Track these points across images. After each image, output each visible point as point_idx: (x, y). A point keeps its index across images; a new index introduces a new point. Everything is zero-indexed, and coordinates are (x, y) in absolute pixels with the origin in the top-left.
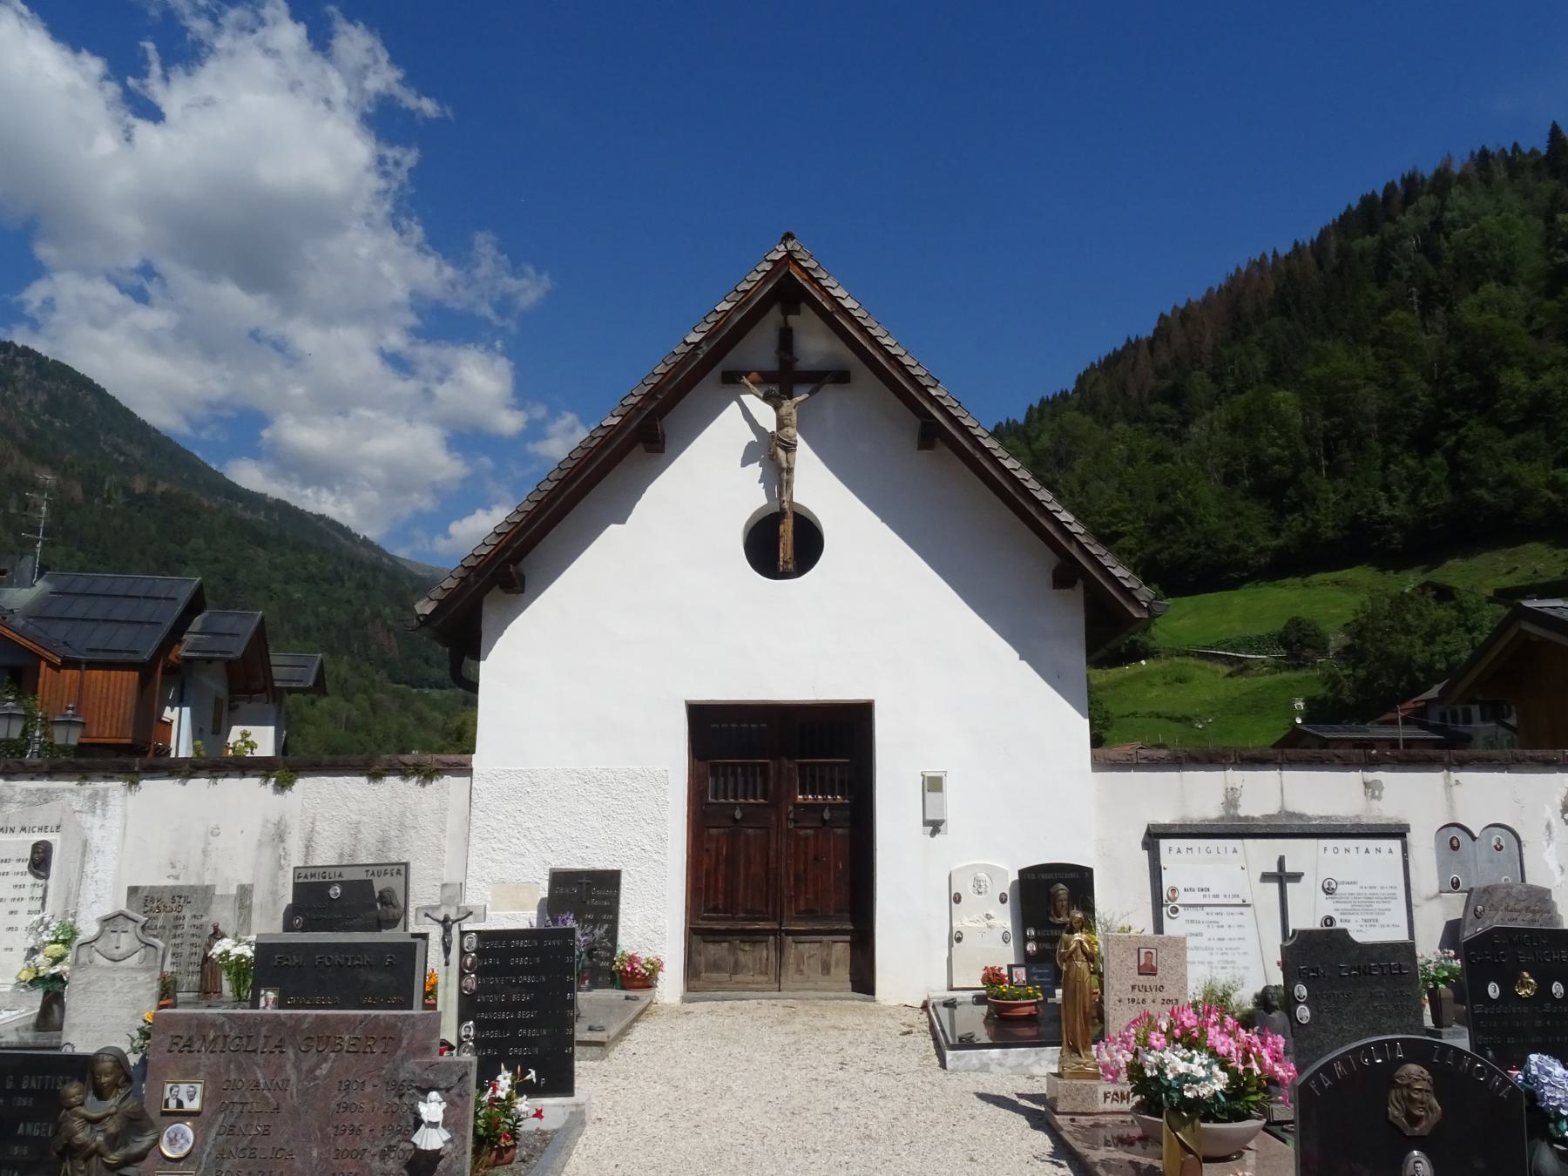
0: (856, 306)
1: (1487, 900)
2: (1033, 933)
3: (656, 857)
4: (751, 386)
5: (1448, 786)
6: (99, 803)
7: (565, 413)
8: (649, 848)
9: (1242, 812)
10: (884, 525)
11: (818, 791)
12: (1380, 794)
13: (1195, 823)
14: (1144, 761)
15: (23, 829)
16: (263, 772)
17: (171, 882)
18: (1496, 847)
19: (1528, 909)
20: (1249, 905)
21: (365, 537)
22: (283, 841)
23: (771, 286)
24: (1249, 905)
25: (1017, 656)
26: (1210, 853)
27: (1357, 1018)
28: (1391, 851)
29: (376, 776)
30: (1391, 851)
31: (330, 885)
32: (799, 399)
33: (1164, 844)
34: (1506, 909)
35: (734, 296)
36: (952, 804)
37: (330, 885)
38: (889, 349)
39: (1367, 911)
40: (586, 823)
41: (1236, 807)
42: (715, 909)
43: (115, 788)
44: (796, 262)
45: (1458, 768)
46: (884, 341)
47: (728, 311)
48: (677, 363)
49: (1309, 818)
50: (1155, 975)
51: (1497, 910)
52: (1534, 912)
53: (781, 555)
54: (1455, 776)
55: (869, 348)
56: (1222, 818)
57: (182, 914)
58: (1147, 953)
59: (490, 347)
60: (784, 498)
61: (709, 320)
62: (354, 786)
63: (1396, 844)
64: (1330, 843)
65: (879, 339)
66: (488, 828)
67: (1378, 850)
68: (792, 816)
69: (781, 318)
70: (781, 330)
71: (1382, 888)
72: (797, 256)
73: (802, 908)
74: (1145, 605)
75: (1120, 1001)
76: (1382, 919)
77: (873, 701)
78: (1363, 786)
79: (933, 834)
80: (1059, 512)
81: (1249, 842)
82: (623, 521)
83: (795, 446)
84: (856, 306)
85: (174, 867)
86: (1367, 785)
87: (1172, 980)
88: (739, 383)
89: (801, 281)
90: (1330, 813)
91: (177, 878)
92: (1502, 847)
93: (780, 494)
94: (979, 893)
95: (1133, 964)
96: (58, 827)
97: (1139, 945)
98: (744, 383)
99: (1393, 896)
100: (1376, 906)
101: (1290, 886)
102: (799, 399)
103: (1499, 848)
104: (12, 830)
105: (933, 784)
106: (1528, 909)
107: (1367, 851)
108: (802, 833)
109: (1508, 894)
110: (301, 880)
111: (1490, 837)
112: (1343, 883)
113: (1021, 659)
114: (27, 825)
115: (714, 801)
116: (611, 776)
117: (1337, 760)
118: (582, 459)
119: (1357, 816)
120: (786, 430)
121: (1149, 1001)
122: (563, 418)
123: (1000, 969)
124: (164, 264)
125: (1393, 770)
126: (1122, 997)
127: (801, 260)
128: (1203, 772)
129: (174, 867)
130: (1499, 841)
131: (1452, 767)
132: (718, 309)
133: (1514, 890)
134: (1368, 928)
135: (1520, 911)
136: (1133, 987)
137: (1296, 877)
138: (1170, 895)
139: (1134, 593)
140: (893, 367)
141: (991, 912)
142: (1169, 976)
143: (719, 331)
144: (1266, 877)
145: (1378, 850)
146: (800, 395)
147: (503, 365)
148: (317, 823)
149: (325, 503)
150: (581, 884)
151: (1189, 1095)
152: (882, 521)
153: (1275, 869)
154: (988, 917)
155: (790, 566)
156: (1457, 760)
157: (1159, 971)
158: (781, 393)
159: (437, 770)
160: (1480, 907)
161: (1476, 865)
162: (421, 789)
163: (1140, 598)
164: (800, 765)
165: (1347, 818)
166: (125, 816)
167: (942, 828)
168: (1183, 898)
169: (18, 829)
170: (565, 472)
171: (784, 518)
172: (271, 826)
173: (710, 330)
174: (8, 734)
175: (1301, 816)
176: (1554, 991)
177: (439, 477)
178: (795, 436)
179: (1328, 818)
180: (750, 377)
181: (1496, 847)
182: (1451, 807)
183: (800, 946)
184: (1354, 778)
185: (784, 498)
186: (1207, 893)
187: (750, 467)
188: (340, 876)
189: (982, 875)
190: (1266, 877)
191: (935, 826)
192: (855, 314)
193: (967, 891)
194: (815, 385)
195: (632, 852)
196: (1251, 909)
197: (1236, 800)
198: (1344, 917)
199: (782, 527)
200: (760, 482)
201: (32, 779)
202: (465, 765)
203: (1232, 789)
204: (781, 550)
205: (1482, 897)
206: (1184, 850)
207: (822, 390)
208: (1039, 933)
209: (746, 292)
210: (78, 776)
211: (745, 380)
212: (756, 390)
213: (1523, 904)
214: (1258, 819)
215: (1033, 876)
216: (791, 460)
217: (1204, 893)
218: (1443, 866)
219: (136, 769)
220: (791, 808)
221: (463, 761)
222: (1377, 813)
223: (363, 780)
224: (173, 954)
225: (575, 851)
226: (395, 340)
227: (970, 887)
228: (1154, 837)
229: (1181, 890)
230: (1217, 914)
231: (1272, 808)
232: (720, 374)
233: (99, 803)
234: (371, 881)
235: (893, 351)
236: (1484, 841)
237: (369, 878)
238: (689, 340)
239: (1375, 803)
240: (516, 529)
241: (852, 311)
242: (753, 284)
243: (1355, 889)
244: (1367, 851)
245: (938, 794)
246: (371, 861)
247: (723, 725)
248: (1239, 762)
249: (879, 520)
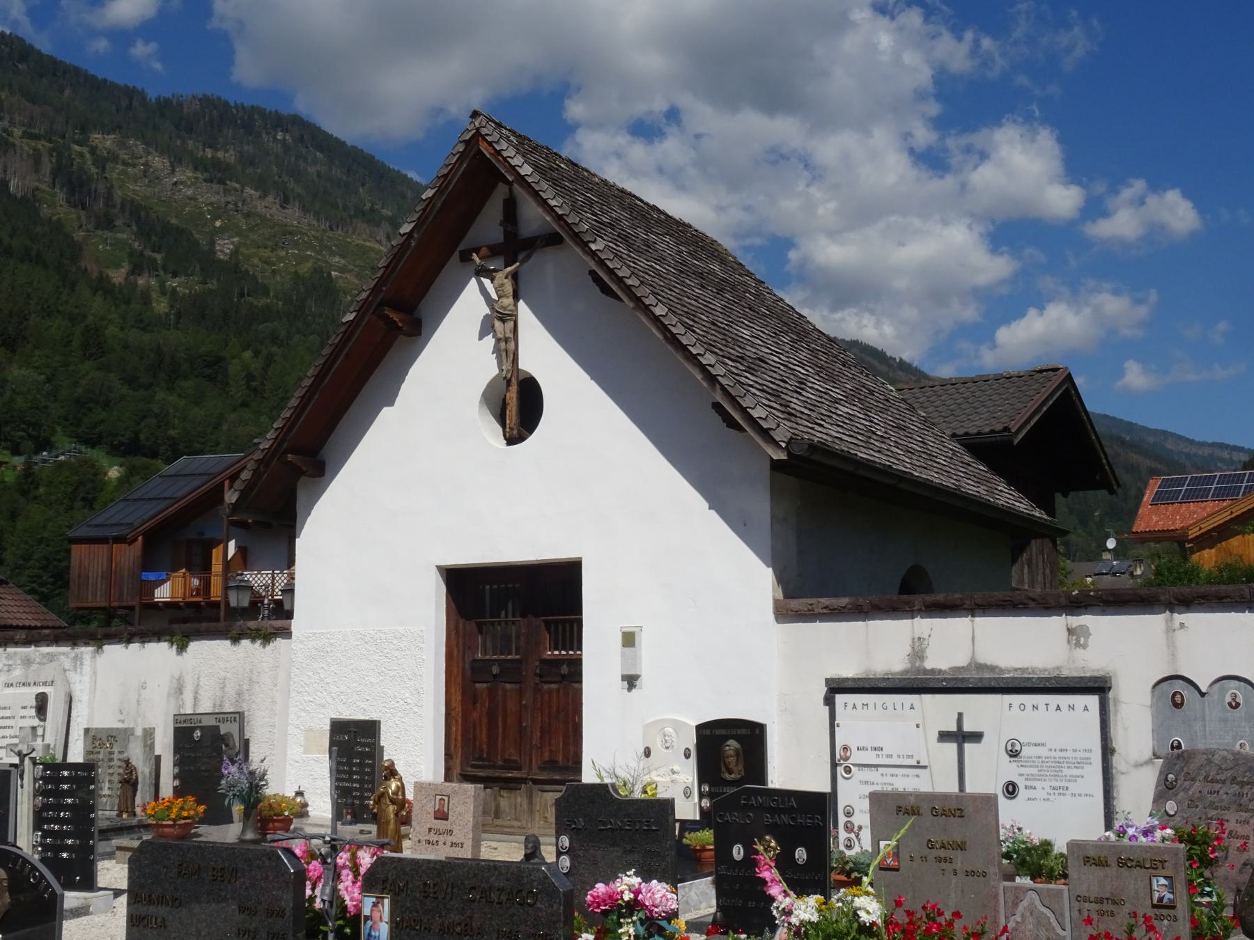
1: (1182, 769)
2: (707, 789)
3: (415, 709)
5: (1170, 631)
6: (79, 663)
7: (1132, 181)
8: (409, 701)
9: (929, 665)
10: (593, 382)
11: (568, 647)
12: (1086, 641)
13: (878, 676)
14: (825, 611)
15: (35, 684)
16: (168, 638)
17: (120, 725)
18: (1230, 704)
19: (1234, 779)
20: (925, 767)
21: (901, 359)
22: (181, 693)
24: (925, 767)
25: (707, 505)
26: (886, 709)
27: (611, 871)
28: (1086, 709)
29: (236, 640)
30: (1086, 709)
31: (194, 729)
33: (840, 699)
34: (1206, 778)
36: (648, 661)
37: (193, 729)
39: (1056, 777)
40: (366, 678)
41: (922, 658)
42: (481, 759)
43: (86, 651)
44: (483, 137)
45: (1183, 608)
46: (553, 203)
49: (1002, 671)
50: (447, 819)
51: (1193, 780)
52: (1242, 784)
54: (1178, 618)
56: (906, 672)
57: (113, 750)
58: (441, 799)
59: (1028, 119)
62: (221, 647)
63: (1093, 701)
64: (1016, 699)
66: (302, 683)
67: (1071, 707)
68: (538, 671)
71: (1075, 751)
72: (484, 131)
73: (547, 759)
74: (783, 445)
75: (419, 841)
76: (1074, 788)
77: (581, 558)
78: (1066, 633)
79: (630, 689)
80: (702, 355)
81: (927, 698)
82: (391, 403)
85: (121, 714)
86: (1070, 631)
87: (460, 825)
90: (1026, 665)
91: (123, 722)
92: (1238, 705)
94: (667, 748)
95: (432, 811)
96: (52, 682)
97: (436, 792)
99: (1087, 761)
100: (1066, 772)
101: (968, 747)
103: (1235, 706)
104: (29, 685)
105: (629, 639)
106: (1234, 779)
107: (1058, 708)
108: (546, 687)
109: (1209, 761)
110: (178, 725)
111: (1223, 692)
112: (1029, 744)
113: (710, 508)
114: (37, 680)
115: (483, 658)
116: (383, 636)
117: (1032, 604)
118: (331, 354)
119: (1058, 668)
121: (441, 843)
122: (1130, 186)
124: (685, 100)
125: (1103, 613)
126: (421, 838)
127: (487, 135)
128: (889, 621)
129: (121, 714)
130: (1234, 696)
131: (1177, 608)
133: (1216, 757)
134: (1056, 796)
135: (1224, 782)
136: (430, 830)
137: (976, 737)
138: (842, 753)
139: (772, 433)
141: (676, 768)
142: (457, 821)
143: (427, 218)
144: (944, 736)
145: (1071, 707)
147: (1046, 138)
148: (201, 679)
149: (866, 326)
150: (350, 732)
152: (592, 379)
153: (954, 728)
154: (673, 772)
156: (1177, 599)
157: (450, 817)
159: (274, 633)
160: (1171, 776)
161: (1204, 726)
162: (262, 650)
163: (777, 439)
164: (544, 621)
165: (1046, 670)
166: (95, 673)
167: (638, 683)
168: (857, 757)
169: (32, 684)
170: (319, 368)
172: (174, 681)
173: (419, 218)
175: (992, 668)
176: (797, 857)
177: (982, 280)
179: (1023, 670)
181: (1230, 704)
182: (1173, 656)
183: (545, 794)
184: (1056, 625)
186: (880, 753)
188: (200, 722)
189: (670, 730)
190: (944, 736)
191: (631, 681)
193: (657, 747)
195: (398, 705)
196: (927, 771)
197: (923, 651)
198: (1029, 783)
200: (493, 353)
201: (48, 646)
202: (287, 629)
203: (919, 639)
204: (507, 417)
205: (1175, 764)
206: (859, 706)
208: (713, 791)
210: (71, 643)
213: (1229, 774)
214: (945, 672)
215: (708, 732)
217: (877, 752)
218: (1160, 729)
219: (99, 637)
220: (537, 663)
221: (286, 627)
222: (1081, 664)
223: (228, 643)
224: (109, 781)
225: (358, 703)
226: (923, 136)
227: (659, 744)
228: (836, 688)
229: (854, 749)
230: (892, 775)
231: (961, 660)
233: (79, 663)
234: (219, 726)
236: (1216, 697)
237: (218, 724)
239: (1079, 652)
240: (289, 423)
242: (450, 167)
243: (1042, 752)
244: (1058, 708)
245: (632, 649)
246: (232, 710)
247: (510, 586)
248: (923, 609)
249: (588, 378)
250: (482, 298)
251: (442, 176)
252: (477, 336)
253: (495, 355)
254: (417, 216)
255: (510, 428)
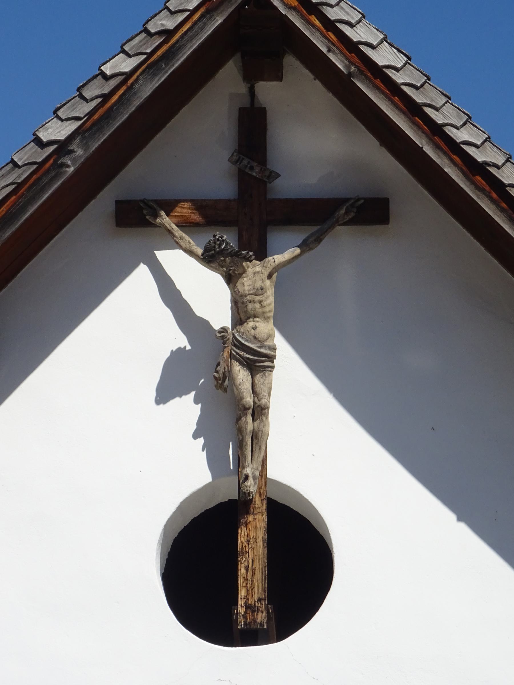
0: (399, 61)
4: (178, 232)
10: (463, 527)
23: (219, 20)
32: (278, 259)
35: (142, 44)
38: (471, 151)
47: (128, 75)
48: (20, 185)
53: (242, 593)
55: (428, 150)
60: (248, 471)
61: (88, 93)
65: (451, 132)
69: (243, 89)
70: (242, 111)
83: (271, 358)
84: (399, 61)
88: (155, 226)
89: (283, 10)
93: (239, 462)
98: (162, 226)
102: (278, 259)
120: (251, 324)
123: (185, 347)
132: (108, 69)
140: (478, 188)
143: (108, 116)
146: (281, 252)
151: (56, 115)
152: (459, 519)
155: (261, 617)
158: (242, 245)
171: (248, 513)
173: (91, 114)
174: (403, 63)
178: (271, 336)
180: (176, 212)
185: (248, 471)
187: (176, 403)
192: (399, 78)
194: (314, 229)
199: (242, 532)
200: (196, 436)
204: (241, 582)
207: (326, 241)
209: (167, 34)
211: (165, 219)
212: (187, 239)
216: (261, 388)
232: (112, 208)
235: (479, 156)
238: (44, 136)
241: (390, 73)
242: (181, 18)
249: (450, 516)
250: (168, 313)
251: (160, 33)
252: (153, 394)
253: (201, 441)
254: (88, 108)
255: (247, 607)
